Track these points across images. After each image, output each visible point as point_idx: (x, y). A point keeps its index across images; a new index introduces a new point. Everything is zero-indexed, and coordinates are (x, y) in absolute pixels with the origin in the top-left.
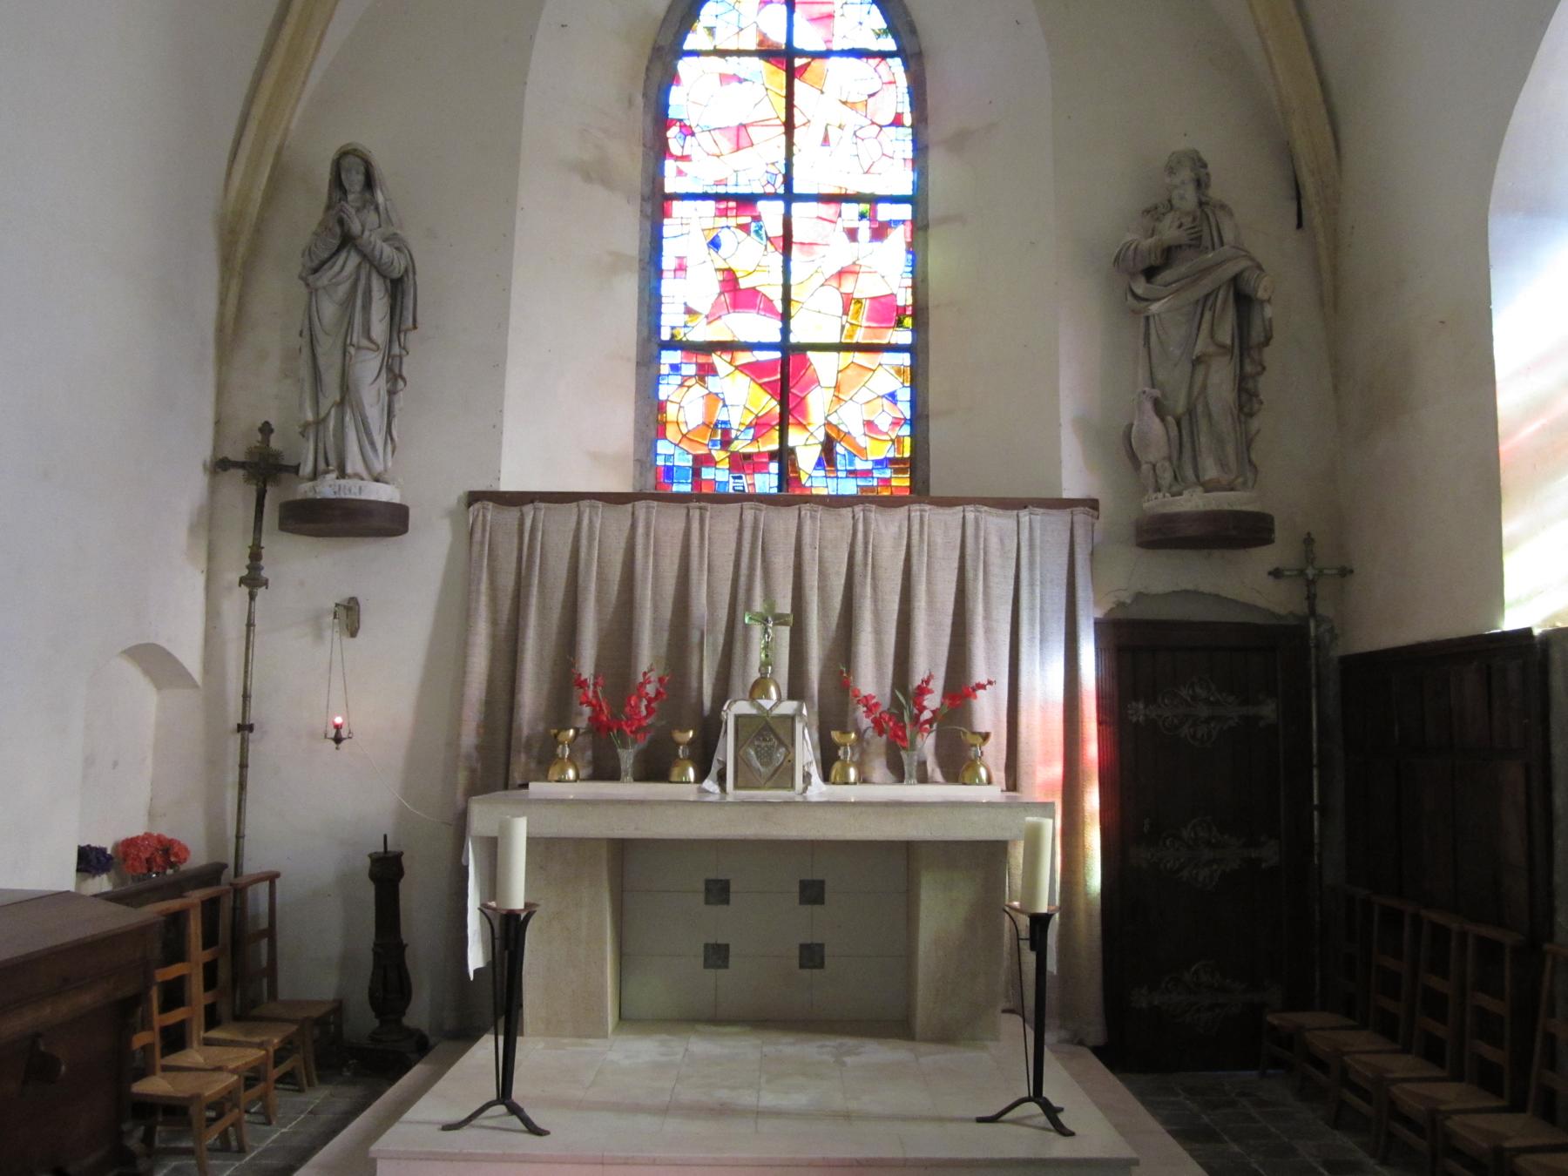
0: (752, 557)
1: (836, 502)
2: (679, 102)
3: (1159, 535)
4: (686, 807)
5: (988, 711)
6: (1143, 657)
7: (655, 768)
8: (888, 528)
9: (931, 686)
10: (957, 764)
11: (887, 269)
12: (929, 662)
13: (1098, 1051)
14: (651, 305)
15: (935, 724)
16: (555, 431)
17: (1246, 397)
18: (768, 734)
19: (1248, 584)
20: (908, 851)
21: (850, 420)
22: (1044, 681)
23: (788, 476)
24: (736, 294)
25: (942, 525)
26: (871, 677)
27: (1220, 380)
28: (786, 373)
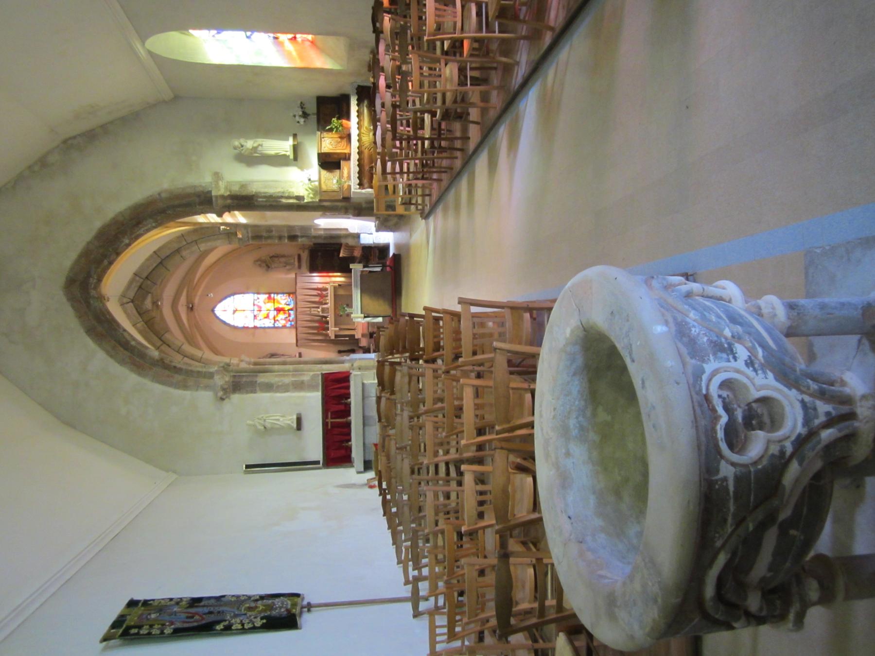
0: (303, 313)
1: (296, 304)
2: (241, 325)
3: (300, 267)
4: (331, 319)
5: (320, 286)
6: (313, 268)
7: (327, 323)
8: (299, 297)
9: (679, 320)
10: (326, 290)
11: (264, 297)
12: (315, 292)
13: (94, 130)
14: (269, 328)
15: (321, 292)
16: (290, 337)
17: (283, 256)
18: (323, 310)
19: (305, 256)
20: (335, 295)
21: (283, 302)
22: (317, 279)
23: (291, 310)
24: (267, 317)
25: (298, 291)
26: (317, 299)
27: (283, 260)
28: (279, 310)
